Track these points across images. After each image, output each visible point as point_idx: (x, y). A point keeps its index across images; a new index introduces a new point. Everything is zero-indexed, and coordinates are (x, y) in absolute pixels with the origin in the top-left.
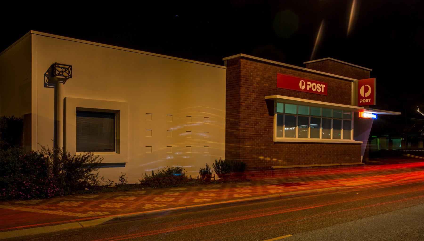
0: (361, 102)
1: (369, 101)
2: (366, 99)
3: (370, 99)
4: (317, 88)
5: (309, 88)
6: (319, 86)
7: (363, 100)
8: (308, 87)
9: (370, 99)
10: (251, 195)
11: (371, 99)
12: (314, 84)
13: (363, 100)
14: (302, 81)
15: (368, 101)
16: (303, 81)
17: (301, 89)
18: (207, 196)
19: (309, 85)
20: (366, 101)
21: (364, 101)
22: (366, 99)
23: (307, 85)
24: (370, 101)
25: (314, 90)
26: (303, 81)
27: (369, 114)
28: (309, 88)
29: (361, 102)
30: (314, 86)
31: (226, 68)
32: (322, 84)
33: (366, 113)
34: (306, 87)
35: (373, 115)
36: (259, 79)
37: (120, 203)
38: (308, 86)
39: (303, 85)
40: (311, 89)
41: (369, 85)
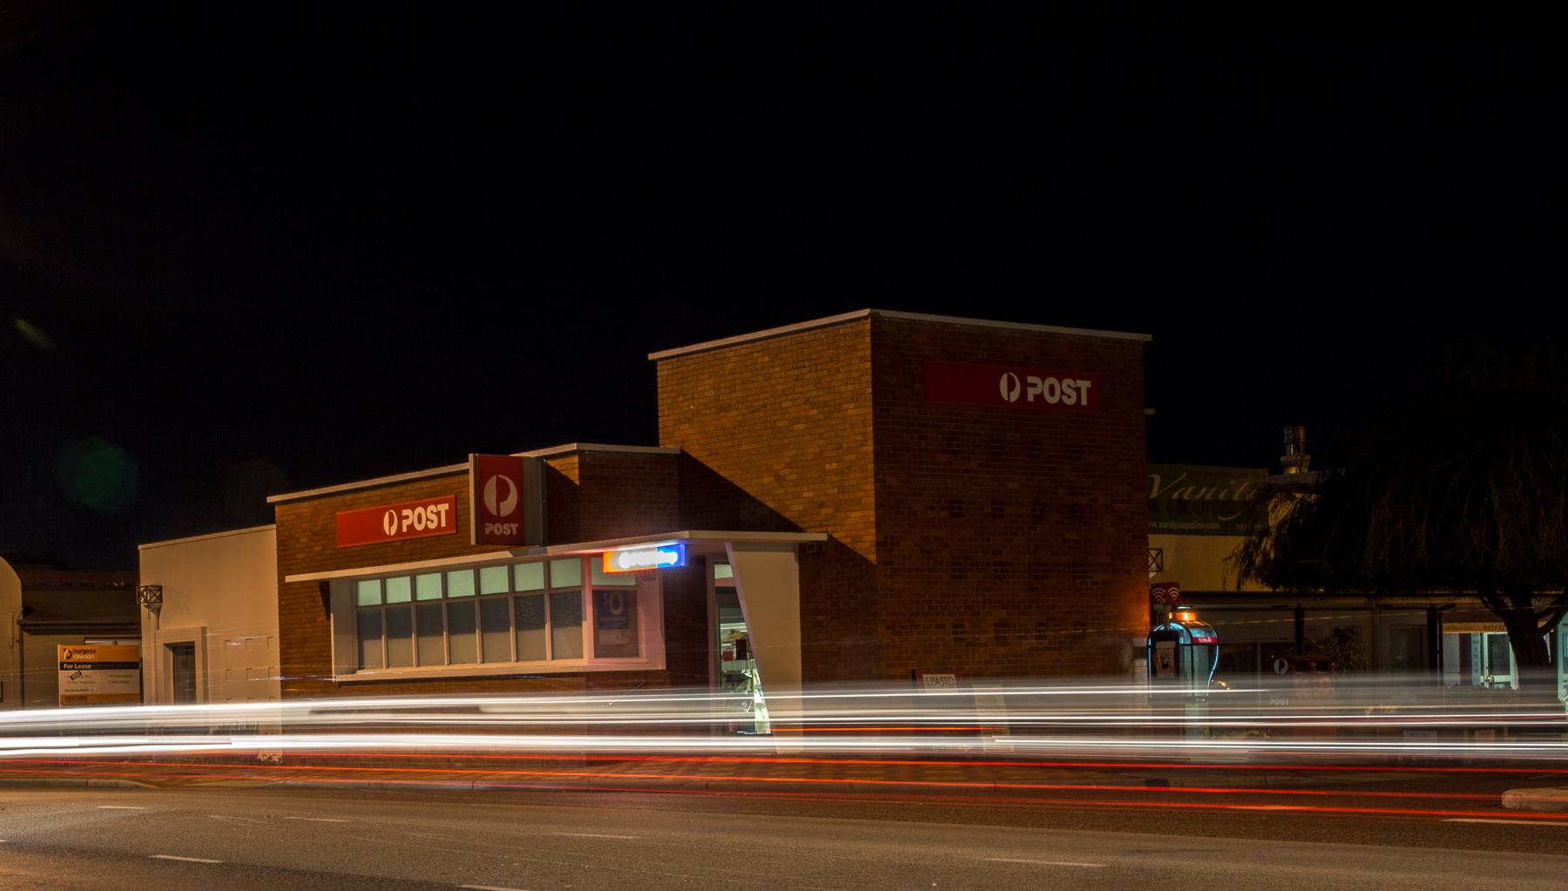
0: (487, 531)
1: (512, 531)
3: (514, 526)
4: (428, 519)
6: (1069, 386)
7: (494, 524)
8: (1031, 393)
9: (514, 526)
10: (239, 644)
11: (517, 525)
12: (1052, 380)
13: (494, 524)
14: (1008, 375)
15: (505, 527)
16: (1013, 375)
17: (1006, 399)
19: (1034, 385)
21: (1052, 390)
23: (1025, 386)
24: (514, 533)
25: (1052, 400)
26: (1013, 375)
27: (641, 553)
29: (487, 531)
31: (1011, 401)
33: (627, 551)
34: (1024, 393)
35: (661, 552)
36: (306, 540)
38: (1029, 389)
39: (1011, 387)
40: (1039, 397)
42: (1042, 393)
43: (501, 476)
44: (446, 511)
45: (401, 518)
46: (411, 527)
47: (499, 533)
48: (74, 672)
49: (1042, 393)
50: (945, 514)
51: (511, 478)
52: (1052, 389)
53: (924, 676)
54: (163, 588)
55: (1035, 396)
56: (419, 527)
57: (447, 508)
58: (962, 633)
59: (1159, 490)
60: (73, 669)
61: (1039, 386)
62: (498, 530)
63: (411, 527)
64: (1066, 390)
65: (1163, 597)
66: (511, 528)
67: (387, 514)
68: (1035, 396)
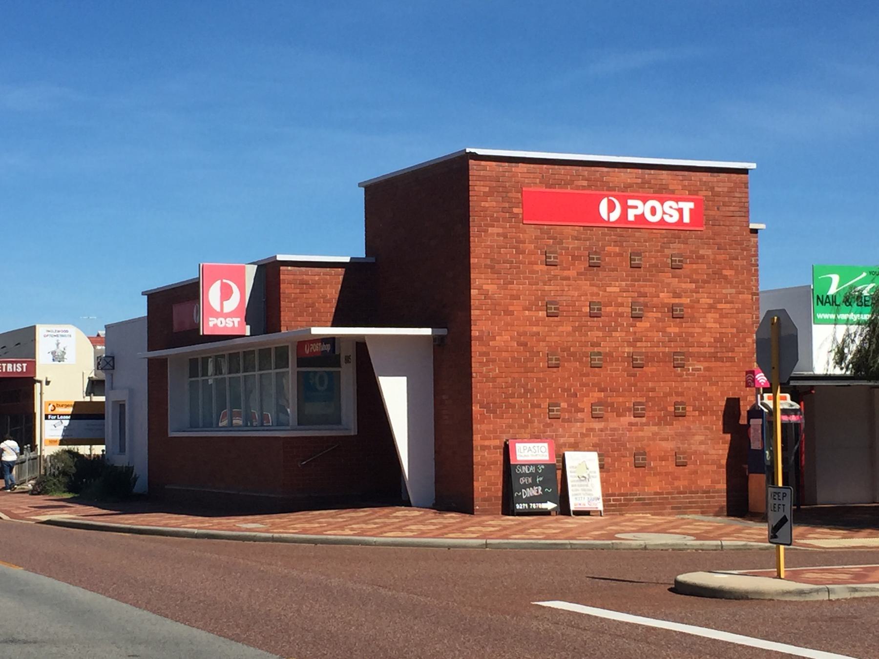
2: (228, 319)
7: (217, 319)
8: (631, 215)
11: (691, 205)
18: (639, 520)
20: (664, 213)
21: (653, 211)
23: (625, 208)
24: (687, 219)
37: (702, 531)
39: (611, 208)
41: (233, 282)
43: (224, 281)
46: (312, 350)
47: (223, 325)
48: (57, 421)
49: (643, 214)
50: (542, 314)
53: (728, 437)
54: (115, 357)
55: (636, 216)
58: (557, 410)
59: (839, 286)
60: (56, 419)
61: (639, 208)
62: (221, 323)
66: (233, 322)
68: (636, 216)
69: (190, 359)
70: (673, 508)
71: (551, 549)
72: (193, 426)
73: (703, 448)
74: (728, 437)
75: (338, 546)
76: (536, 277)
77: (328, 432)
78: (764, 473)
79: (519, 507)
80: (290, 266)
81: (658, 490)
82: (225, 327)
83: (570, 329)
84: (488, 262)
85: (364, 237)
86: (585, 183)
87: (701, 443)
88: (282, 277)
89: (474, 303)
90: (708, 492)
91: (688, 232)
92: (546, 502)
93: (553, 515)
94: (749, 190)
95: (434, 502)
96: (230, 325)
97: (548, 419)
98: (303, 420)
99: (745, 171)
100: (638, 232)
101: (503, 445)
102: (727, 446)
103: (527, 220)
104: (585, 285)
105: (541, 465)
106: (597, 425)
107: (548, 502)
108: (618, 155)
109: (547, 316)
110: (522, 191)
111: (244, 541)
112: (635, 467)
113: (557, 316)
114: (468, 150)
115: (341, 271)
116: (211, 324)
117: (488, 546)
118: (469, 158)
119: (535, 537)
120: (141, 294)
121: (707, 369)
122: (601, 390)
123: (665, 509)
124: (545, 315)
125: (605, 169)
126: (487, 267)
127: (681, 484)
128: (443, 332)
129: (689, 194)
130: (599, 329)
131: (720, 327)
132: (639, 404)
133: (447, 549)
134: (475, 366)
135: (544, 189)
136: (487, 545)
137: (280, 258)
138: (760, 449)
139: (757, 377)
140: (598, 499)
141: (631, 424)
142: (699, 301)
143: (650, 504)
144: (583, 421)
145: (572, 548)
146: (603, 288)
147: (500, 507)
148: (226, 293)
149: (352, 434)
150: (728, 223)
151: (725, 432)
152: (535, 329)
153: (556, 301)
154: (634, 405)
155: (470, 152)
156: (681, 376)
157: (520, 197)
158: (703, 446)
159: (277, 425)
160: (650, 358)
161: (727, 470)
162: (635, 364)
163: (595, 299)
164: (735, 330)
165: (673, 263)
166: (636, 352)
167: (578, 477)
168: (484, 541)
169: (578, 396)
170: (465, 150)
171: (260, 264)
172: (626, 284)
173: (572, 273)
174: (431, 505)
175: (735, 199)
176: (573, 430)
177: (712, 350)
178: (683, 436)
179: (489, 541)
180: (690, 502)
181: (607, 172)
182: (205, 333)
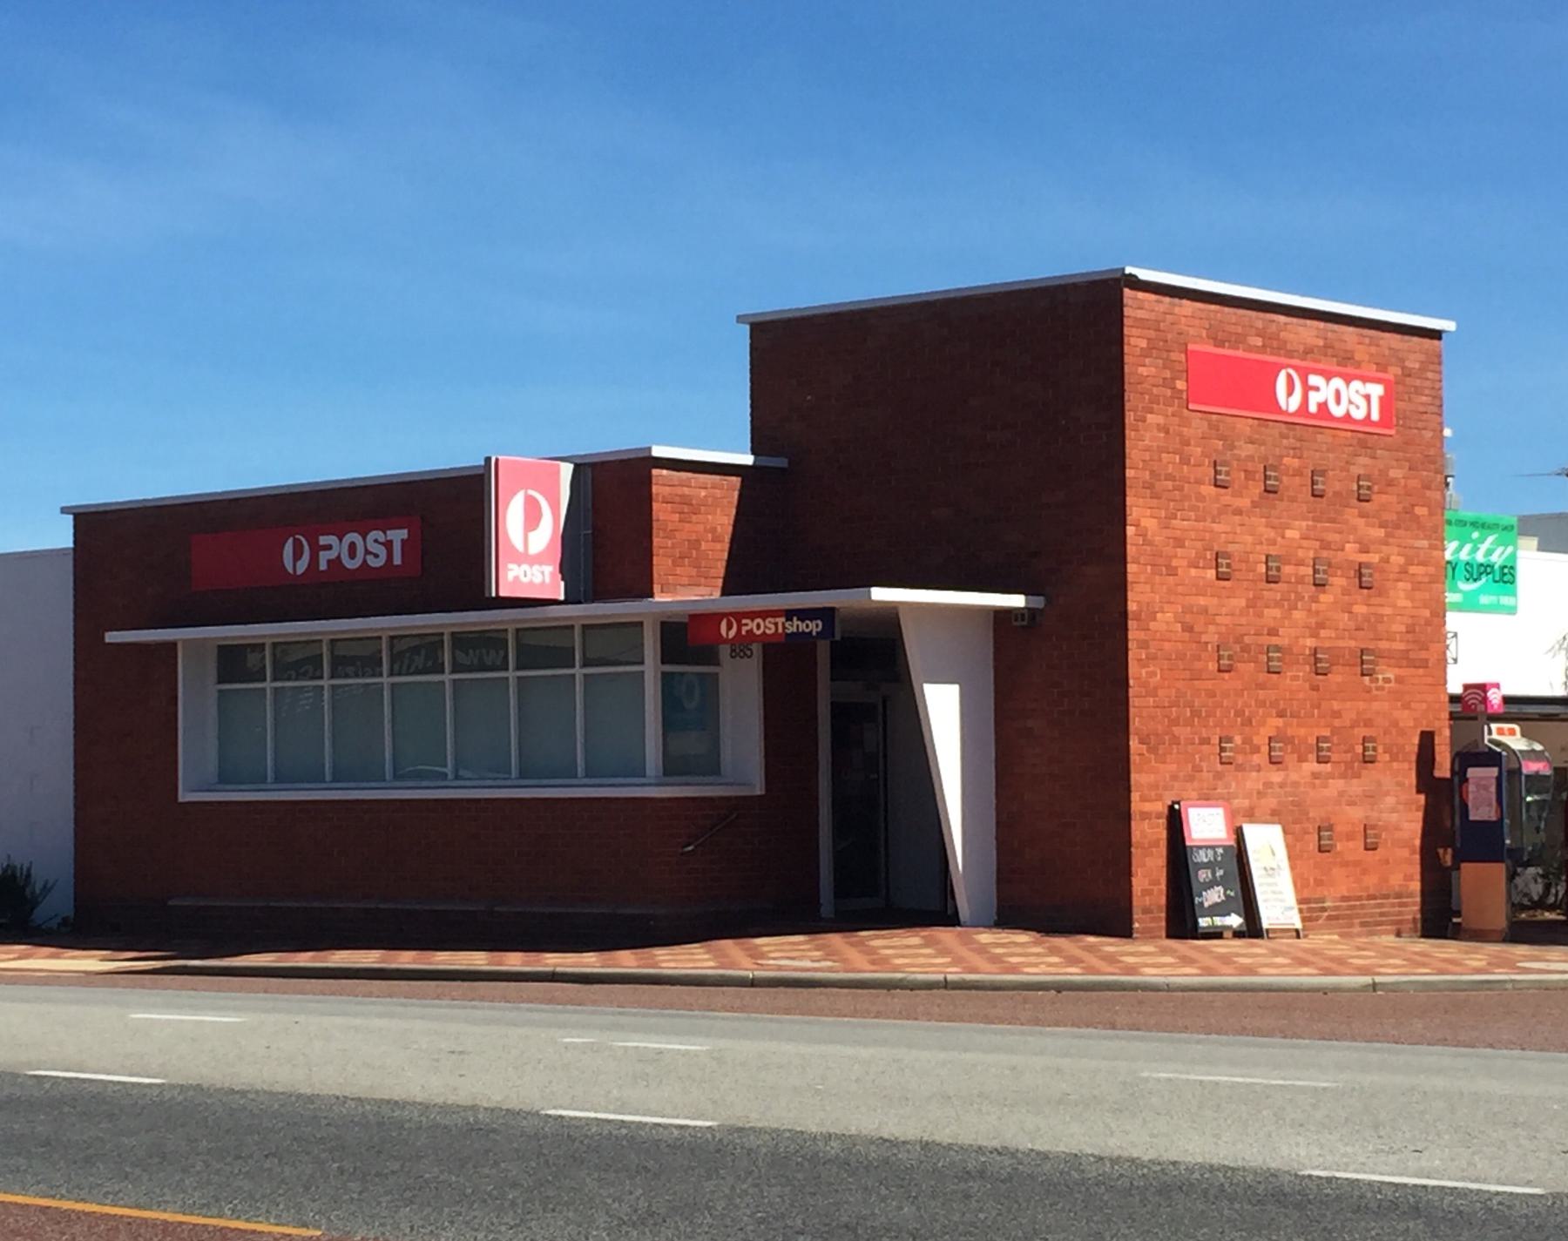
2: (767, 621)
4: (367, 552)
5: (329, 562)
8: (1314, 399)
11: (403, 534)
19: (1317, 389)
21: (758, 626)
22: (764, 620)
23: (316, 549)
25: (351, 564)
28: (329, 562)
30: (352, 548)
32: (390, 529)
34: (314, 559)
39: (297, 555)
41: (547, 499)
42: (339, 557)
43: (532, 492)
44: (402, 540)
45: (1307, 388)
46: (1323, 406)
51: (541, 493)
52: (352, 548)
53: (1422, 797)
56: (1338, 411)
57: (406, 537)
63: (1323, 406)
64: (373, 547)
65: (1481, 702)
67: (290, 540)
69: (219, 646)
70: (1363, 924)
71: (1481, 990)
72: (225, 778)
73: (1394, 817)
74: (1422, 797)
75: (1094, 993)
76: (1204, 507)
77: (656, 789)
78: (1501, 861)
79: (1204, 922)
80: (667, 469)
81: (1346, 894)
82: (531, 583)
83: (1243, 603)
84: (1147, 475)
85: (749, 418)
86: (1259, 342)
87: (1393, 810)
88: (655, 489)
89: (1131, 550)
90: (1399, 896)
91: (1376, 437)
92: (1229, 914)
93: (1227, 939)
94: (1444, 368)
95: (996, 918)
96: (538, 579)
97: (1219, 765)
98: (674, 767)
99: (1436, 335)
100: (1321, 433)
101: (1166, 811)
102: (1420, 815)
103: (1197, 402)
104: (1259, 523)
105: (1218, 846)
106: (1276, 777)
107: (1233, 915)
108: (1303, 295)
109: (1218, 578)
110: (1187, 350)
111: (889, 990)
112: (1320, 851)
113: (1228, 580)
114: (1129, 270)
115: (736, 481)
116: (511, 576)
117: (1377, 988)
118: (1122, 283)
119: (1390, 971)
120: (59, 510)
121: (1399, 680)
122: (1281, 715)
123: (1351, 925)
124: (1214, 577)
125: (1282, 319)
126: (1146, 485)
127: (1371, 881)
128: (1039, 602)
129: (1377, 371)
130: (1278, 604)
131: (1413, 607)
132: (1326, 739)
133: (1321, 993)
134: (1133, 669)
135: (1210, 349)
136: (1374, 986)
137: (659, 451)
138: (1494, 819)
139: (1489, 694)
140: (1292, 908)
141: (1315, 775)
142: (1388, 559)
143: (1336, 918)
144: (1259, 769)
145: (1514, 989)
146: (1281, 528)
147: (1163, 924)
148: (532, 517)
149: (759, 793)
150: (1420, 425)
151: (1419, 792)
152: (1202, 601)
153: (1226, 552)
154: (1318, 742)
155: (1130, 275)
156: (1369, 691)
157: (1184, 360)
158: (1395, 815)
159: (587, 776)
160: (1336, 657)
161: (1422, 859)
162: (1318, 665)
163: (1273, 551)
164: (1427, 613)
165: (1361, 492)
166: (1321, 648)
167: (1265, 869)
168: (1368, 980)
169: (1254, 724)
170: (1123, 269)
171: (578, 461)
172: (1307, 525)
173: (1244, 503)
174: (992, 923)
175: (1428, 383)
176: (1249, 785)
177: (1402, 646)
178: (1371, 798)
179: (1378, 979)
180: (1382, 914)
181: (1286, 324)
182: (502, 594)
